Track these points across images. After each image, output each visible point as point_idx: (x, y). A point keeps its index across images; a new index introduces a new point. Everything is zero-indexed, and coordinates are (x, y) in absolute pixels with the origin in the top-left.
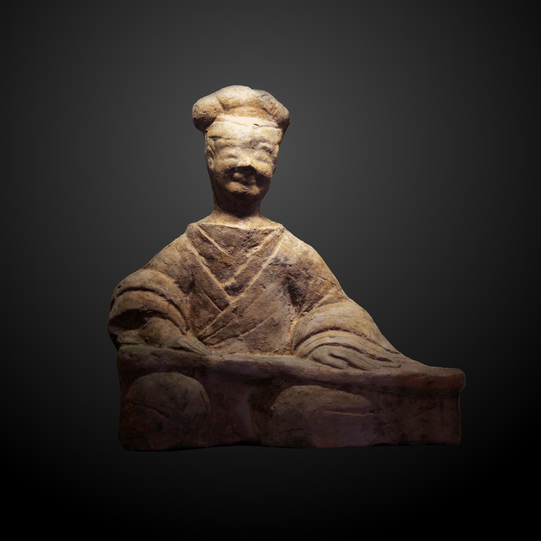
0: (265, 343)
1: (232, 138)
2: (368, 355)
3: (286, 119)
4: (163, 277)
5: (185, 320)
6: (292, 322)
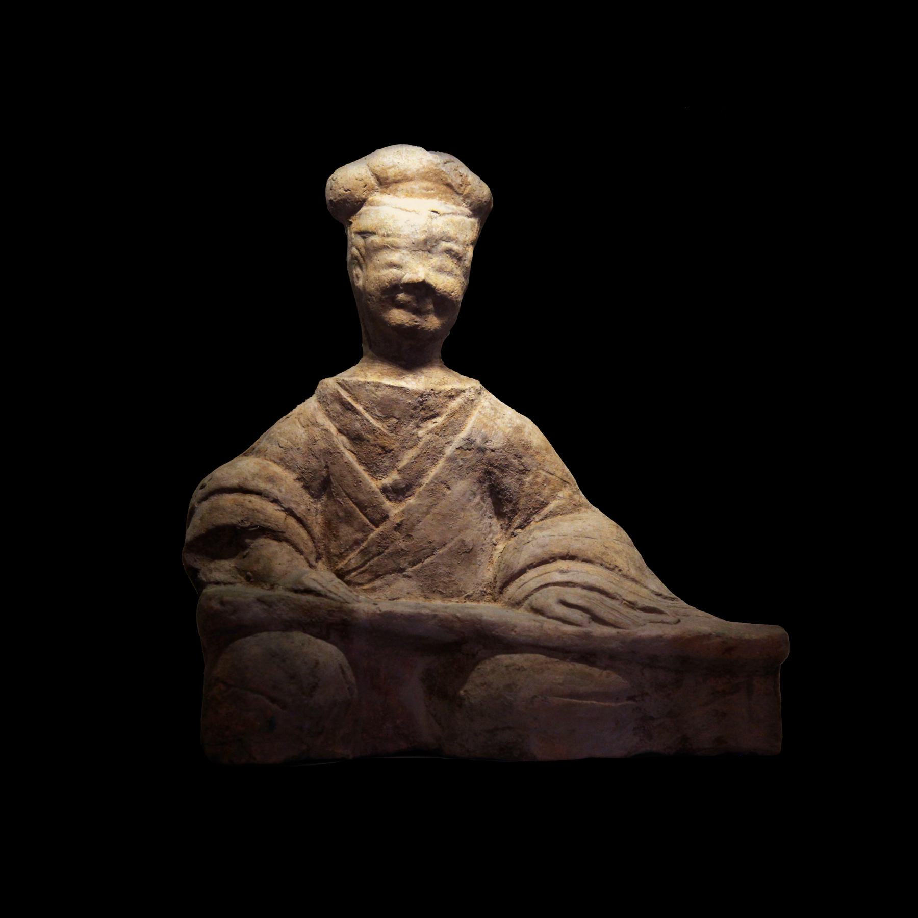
0: (450, 582)
1: (394, 234)
2: (624, 602)
3: (485, 202)
4: (277, 469)
5: (314, 542)
6: (496, 547)
